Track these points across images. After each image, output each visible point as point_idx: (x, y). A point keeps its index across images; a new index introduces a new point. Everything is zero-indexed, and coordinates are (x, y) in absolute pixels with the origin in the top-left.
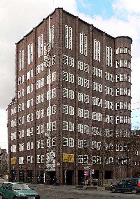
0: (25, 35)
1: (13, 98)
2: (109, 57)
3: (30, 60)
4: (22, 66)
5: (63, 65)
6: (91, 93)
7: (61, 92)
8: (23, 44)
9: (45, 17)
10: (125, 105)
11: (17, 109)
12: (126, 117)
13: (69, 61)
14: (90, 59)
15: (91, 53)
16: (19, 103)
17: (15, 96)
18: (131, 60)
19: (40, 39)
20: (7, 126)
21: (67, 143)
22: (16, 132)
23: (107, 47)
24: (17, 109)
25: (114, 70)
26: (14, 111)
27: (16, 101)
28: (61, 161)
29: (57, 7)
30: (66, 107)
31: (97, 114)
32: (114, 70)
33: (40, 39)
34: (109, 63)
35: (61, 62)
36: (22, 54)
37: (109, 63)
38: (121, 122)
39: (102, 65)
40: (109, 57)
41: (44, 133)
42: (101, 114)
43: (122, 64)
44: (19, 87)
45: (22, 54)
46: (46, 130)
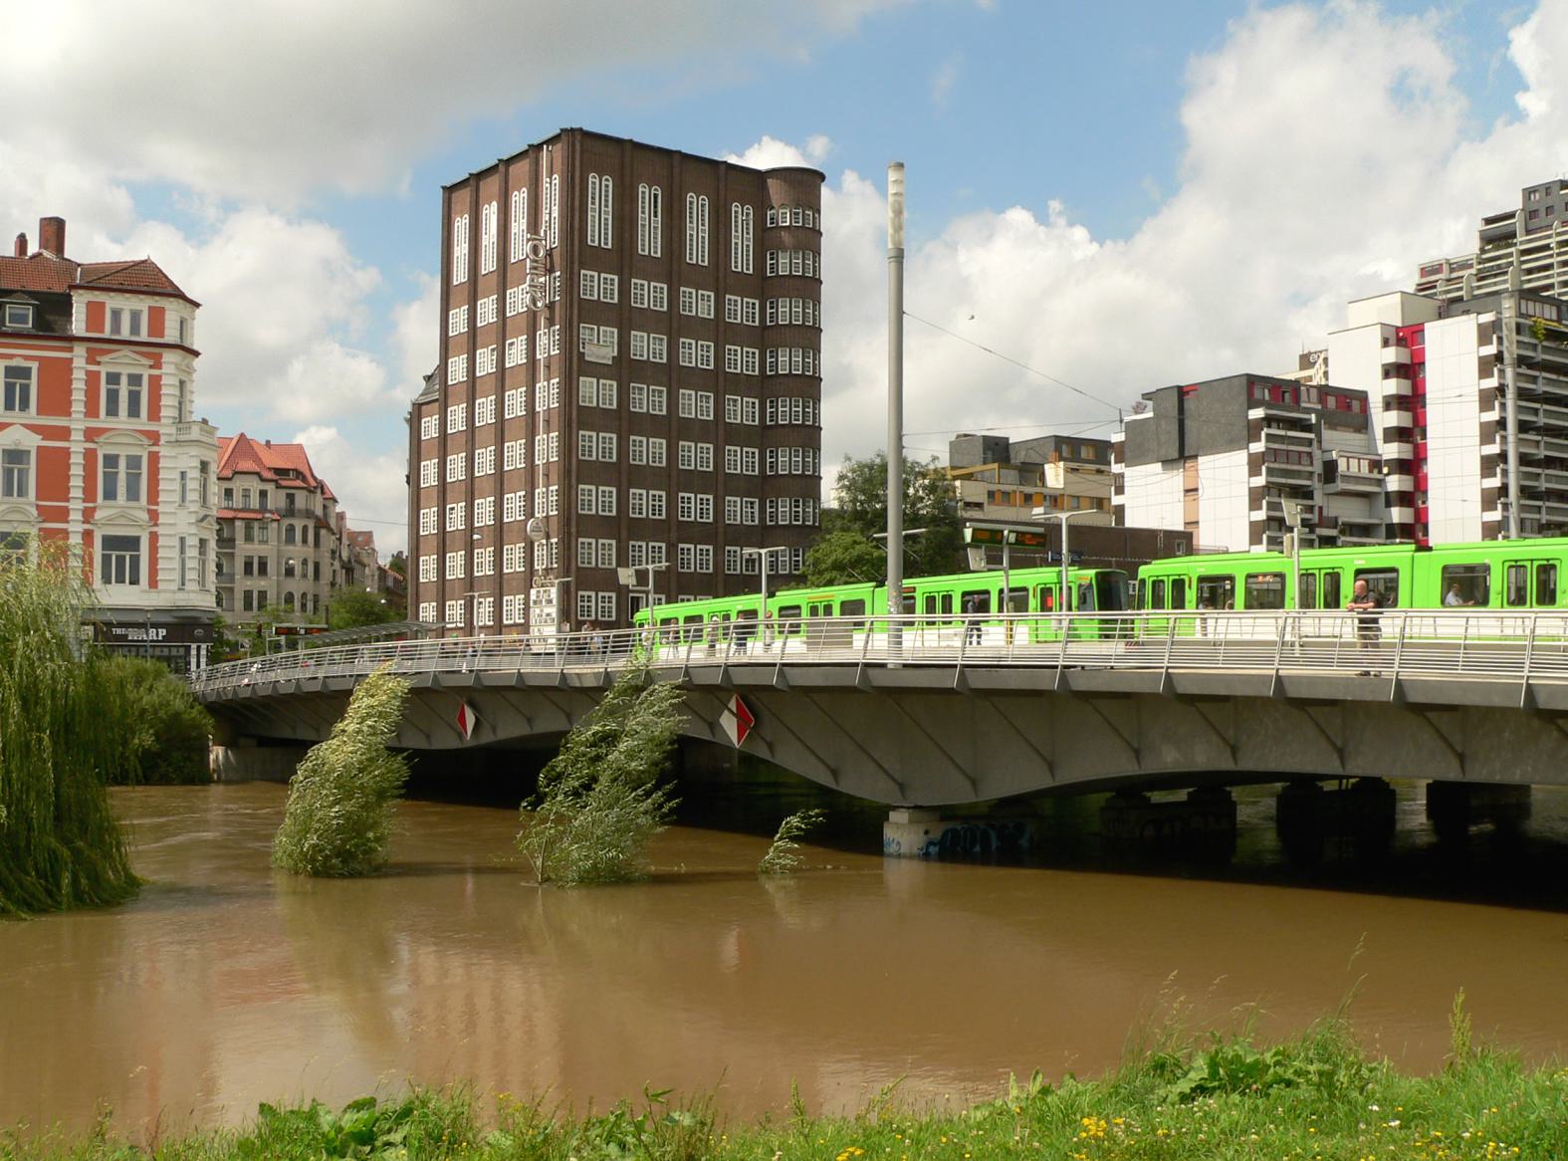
0: (474, 172)
1: (430, 374)
2: (742, 240)
3: (488, 263)
4: (460, 275)
5: (579, 303)
6: (673, 428)
7: (573, 551)
8: (464, 197)
9: (536, 142)
10: (793, 559)
11: (443, 424)
12: (798, 501)
13: (600, 285)
14: (672, 268)
15: (675, 246)
16: (450, 401)
17: (438, 363)
18: (820, 250)
19: (519, 199)
20: (408, 482)
21: (594, 503)
22: (439, 458)
23: (735, 207)
24: (443, 424)
25: (763, 286)
26: (430, 427)
27: (438, 392)
28: (573, 616)
29: (568, 126)
30: (592, 276)
31: (696, 448)
32: (763, 286)
33: (519, 199)
34: (742, 259)
35: (573, 511)
36: (462, 224)
37: (742, 259)
38: (782, 520)
39: (718, 277)
40: (742, 240)
41: (525, 522)
42: (711, 446)
43: (785, 264)
44: (451, 343)
45: (462, 224)
46: (530, 512)
